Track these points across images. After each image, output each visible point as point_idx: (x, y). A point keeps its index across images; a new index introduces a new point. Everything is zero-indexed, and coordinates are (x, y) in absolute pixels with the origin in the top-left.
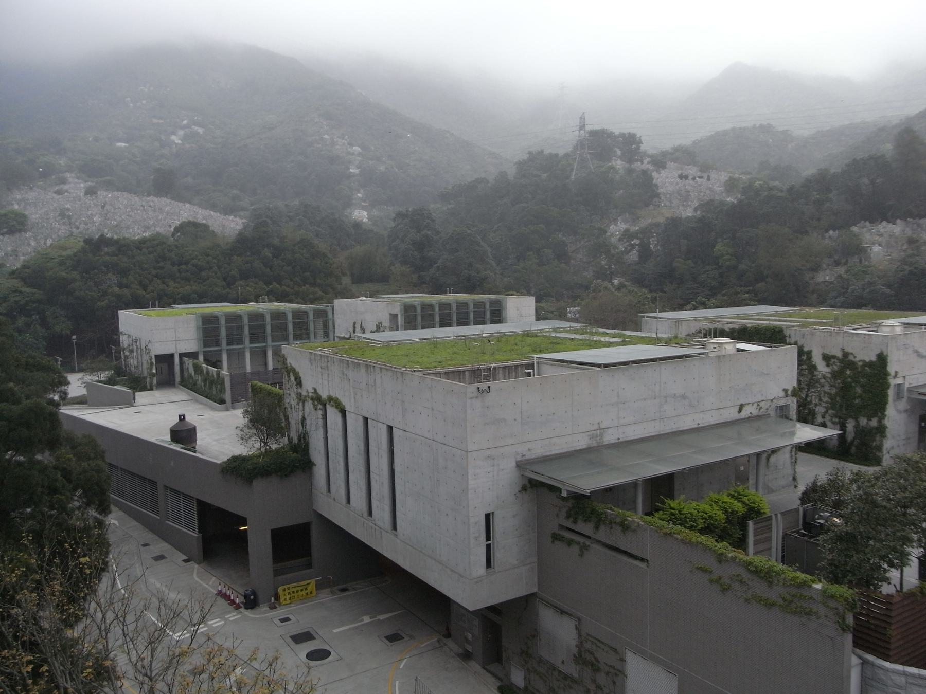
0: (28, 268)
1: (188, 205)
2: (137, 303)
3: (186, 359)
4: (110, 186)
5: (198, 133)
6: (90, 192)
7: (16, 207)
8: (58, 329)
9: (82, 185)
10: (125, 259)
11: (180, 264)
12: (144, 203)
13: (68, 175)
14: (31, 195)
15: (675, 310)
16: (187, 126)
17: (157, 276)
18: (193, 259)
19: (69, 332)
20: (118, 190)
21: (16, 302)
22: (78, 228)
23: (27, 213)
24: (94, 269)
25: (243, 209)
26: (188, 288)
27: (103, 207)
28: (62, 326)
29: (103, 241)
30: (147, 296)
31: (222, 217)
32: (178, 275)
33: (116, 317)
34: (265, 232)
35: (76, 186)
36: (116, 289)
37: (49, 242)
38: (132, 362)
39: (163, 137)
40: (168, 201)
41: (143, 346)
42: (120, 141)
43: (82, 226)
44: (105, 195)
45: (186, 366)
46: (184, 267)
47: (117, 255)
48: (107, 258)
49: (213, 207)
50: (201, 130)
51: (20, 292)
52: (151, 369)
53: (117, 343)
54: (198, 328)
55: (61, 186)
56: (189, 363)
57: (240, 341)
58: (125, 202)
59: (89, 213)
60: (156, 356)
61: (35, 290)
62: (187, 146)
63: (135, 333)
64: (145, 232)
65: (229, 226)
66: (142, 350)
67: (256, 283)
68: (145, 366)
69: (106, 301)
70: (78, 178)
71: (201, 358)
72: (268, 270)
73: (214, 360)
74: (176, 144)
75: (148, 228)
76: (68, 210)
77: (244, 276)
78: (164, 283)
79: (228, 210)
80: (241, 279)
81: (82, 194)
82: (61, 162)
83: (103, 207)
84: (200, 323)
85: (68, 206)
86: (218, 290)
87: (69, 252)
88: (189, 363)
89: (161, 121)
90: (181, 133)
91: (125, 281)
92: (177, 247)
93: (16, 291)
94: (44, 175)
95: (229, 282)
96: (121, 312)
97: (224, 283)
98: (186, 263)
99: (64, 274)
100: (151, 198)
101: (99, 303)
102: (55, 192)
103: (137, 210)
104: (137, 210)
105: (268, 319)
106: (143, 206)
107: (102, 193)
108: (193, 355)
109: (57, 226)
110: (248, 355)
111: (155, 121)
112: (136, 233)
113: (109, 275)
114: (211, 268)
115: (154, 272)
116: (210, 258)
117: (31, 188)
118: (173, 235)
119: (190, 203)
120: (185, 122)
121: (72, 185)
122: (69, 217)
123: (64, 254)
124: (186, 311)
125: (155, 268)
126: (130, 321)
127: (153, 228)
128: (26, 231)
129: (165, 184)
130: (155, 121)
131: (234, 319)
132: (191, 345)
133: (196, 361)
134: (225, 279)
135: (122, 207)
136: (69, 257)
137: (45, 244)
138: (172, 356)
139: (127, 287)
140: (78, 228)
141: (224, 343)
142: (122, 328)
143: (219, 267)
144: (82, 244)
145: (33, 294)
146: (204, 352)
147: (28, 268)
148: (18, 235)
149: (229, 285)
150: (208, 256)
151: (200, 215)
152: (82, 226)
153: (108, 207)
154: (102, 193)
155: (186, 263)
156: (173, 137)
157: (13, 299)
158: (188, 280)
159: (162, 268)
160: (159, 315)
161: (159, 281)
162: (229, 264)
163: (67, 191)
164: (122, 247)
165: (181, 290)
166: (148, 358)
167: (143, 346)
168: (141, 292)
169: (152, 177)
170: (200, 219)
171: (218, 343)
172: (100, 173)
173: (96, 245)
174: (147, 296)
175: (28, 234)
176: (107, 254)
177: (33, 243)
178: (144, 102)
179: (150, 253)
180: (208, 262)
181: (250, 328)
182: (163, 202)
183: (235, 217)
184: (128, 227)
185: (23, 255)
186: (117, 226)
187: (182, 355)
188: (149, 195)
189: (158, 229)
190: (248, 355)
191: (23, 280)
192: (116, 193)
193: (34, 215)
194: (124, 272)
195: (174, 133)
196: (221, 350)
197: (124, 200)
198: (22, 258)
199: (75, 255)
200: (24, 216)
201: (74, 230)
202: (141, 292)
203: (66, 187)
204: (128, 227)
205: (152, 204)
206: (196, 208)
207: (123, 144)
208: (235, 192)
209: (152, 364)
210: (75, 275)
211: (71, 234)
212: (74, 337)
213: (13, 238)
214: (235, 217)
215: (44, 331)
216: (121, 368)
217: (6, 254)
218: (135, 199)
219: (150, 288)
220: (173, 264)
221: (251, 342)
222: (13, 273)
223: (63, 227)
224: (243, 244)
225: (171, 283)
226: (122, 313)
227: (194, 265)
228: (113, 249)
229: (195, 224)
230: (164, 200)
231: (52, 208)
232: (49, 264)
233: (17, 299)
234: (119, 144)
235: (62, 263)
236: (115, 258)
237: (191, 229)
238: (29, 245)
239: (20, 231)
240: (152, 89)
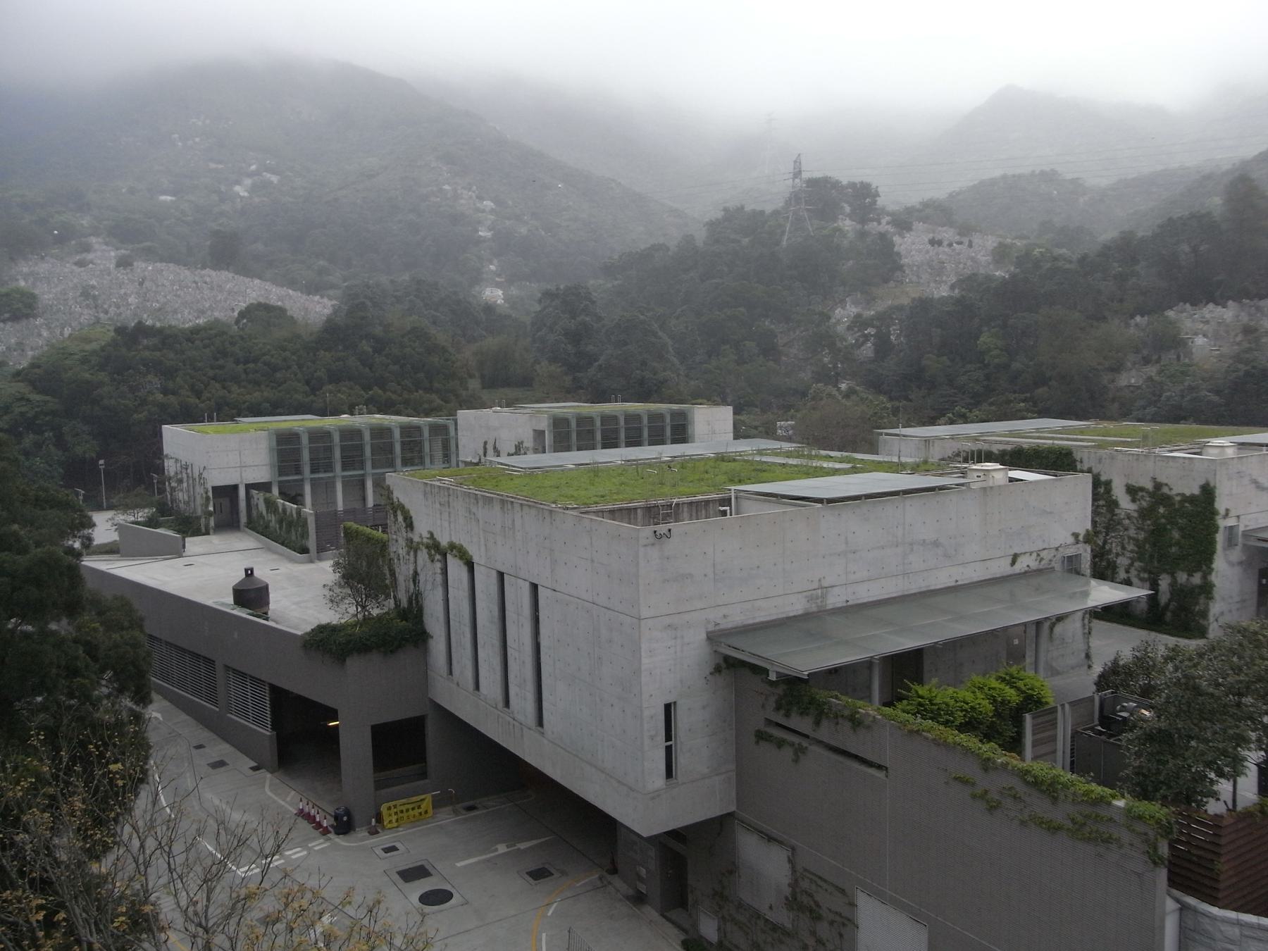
0: (39, 367)
1: (257, 281)
2: (187, 416)
3: (254, 492)
4: (150, 254)
5: (272, 183)
6: (123, 263)
7: (22, 283)
8: (79, 450)
9: (113, 254)
10: (172, 355)
11: (246, 362)
12: (197, 279)
13: (93, 240)
14: (43, 268)
15: (924, 425)
16: (257, 173)
17: (214, 378)
18: (264, 354)
19: (94, 455)
20: (161, 260)
21: (22, 414)
22: (106, 312)
23: (36, 292)
24: (129, 368)
25: (333, 286)
26: (257, 394)
27: (141, 284)
28: (85, 447)
29: (141, 330)
30: (202, 405)
31: (304, 297)
32: (243, 376)
33: (158, 435)
34: (363, 318)
35: (104, 255)
36: (159, 397)
37: (67, 332)
38: (181, 496)
39: (223, 188)
40: (231, 275)
41: (196, 475)
42: (165, 193)
43: (112, 310)
44: (143, 267)
45: (254, 501)
46: (251, 366)
47: (160, 350)
48: (147, 353)
49: (292, 283)
50: (275, 179)
51: (28, 400)
52: (207, 506)
53: (161, 470)
54: (271, 450)
55: (84, 255)
56: (259, 497)
57: (329, 467)
58: (171, 277)
59: (122, 291)
60: (213, 488)
61: (48, 398)
62: (257, 200)
63: (185, 457)
64: (198, 317)
65: (314, 309)
66: (194, 480)
67: (351, 388)
68: (199, 501)
69: (145, 413)
70: (107, 244)
71: (275, 491)
72: (367, 370)
73: (293, 493)
74: (242, 198)
75: (203, 312)
76: (93, 287)
77: (335, 378)
78: (224, 388)
79: (313, 288)
80: (330, 383)
81: (112, 266)
82: (84, 222)
83: (141, 284)
84: (274, 443)
85: (93, 282)
86: (299, 397)
87: (95, 346)
88: (259, 497)
89: (220, 166)
90: (248, 182)
91: (171, 385)
92: (242, 338)
93: (22, 399)
94: (61, 240)
95: (314, 386)
96: (165, 427)
97: (307, 388)
98: (255, 361)
99: (87, 376)
100: (207, 271)
101: (135, 416)
102: (76, 264)
103: (188, 287)
104: (188, 287)
105: (367, 437)
106: (195, 282)
107: (139, 265)
108: (264, 487)
109: (78, 309)
110: (339, 487)
111: (212, 166)
112: (186, 319)
113: (150, 377)
114: (289, 367)
115: (211, 373)
116: (288, 353)
117: (43, 258)
118: (237, 322)
119: (260, 278)
120: (253, 167)
121: (99, 253)
122: (95, 298)
123: (88, 347)
124: (255, 426)
125: (212, 368)
126: (178, 440)
127: (209, 313)
128: (35, 317)
129: (225, 252)
130: (212, 166)
131: (320, 437)
132: (261, 473)
133: (268, 495)
134: (308, 383)
135: (167, 284)
136: (94, 352)
137: (62, 334)
138: (235, 487)
139: (174, 393)
140: (106, 312)
141: (307, 470)
142: (167, 449)
143: (300, 366)
144: (113, 334)
145: (46, 402)
146: (280, 482)
147: (39, 367)
148: (24, 322)
149: (314, 391)
150: (285, 350)
151: (274, 294)
152: (112, 310)
153: (147, 284)
154: (139, 265)
155: (255, 361)
156: (237, 188)
157: (17, 410)
158: (257, 383)
159: (221, 367)
160: (218, 432)
161: (217, 385)
162: (314, 362)
163: (91, 262)
164: (167, 338)
165: (248, 397)
166: (202, 491)
167: (196, 475)
168: (193, 400)
169: (208, 243)
170: (274, 300)
171: (298, 470)
172: (137, 237)
173: (132, 335)
174: (202, 405)
175: (39, 321)
176: (147, 348)
177: (45, 334)
178: (197, 140)
179: (205, 347)
180: (285, 360)
181: (343, 449)
182: (223, 277)
183: (322, 297)
184: (175, 312)
185: (32, 349)
186: (160, 309)
187: (249, 487)
188: (204, 267)
189: (216, 314)
190: (339, 487)
191: (32, 383)
192: (158, 265)
193: (46, 295)
194: (169, 373)
195: (238, 182)
196: (302, 480)
197: (170, 273)
198: (30, 353)
199: (103, 349)
200: (33, 297)
201: (102, 315)
202: (193, 400)
203: (90, 256)
204: (175, 312)
205: (208, 279)
206: (268, 285)
207: (169, 198)
208: (321, 263)
209: (208, 498)
210: (103, 376)
211: (98, 321)
212: (101, 462)
213: (18, 326)
214: (322, 297)
215: (60, 453)
216: (165, 504)
217: (9, 348)
218: (185, 273)
219: (206, 395)
220: (237, 362)
221: (344, 469)
222: (18, 374)
223: (86, 311)
224: (333, 334)
225: (235, 388)
226: (167, 429)
227: (265, 364)
228: (155, 341)
229: (267, 308)
230: (225, 275)
231: (71, 285)
232: (67, 362)
233: (23, 409)
234: (163, 198)
235: (84, 361)
236: (158, 354)
237: (261, 313)
238: (40, 335)
239: (27, 316)
240: (208, 122)
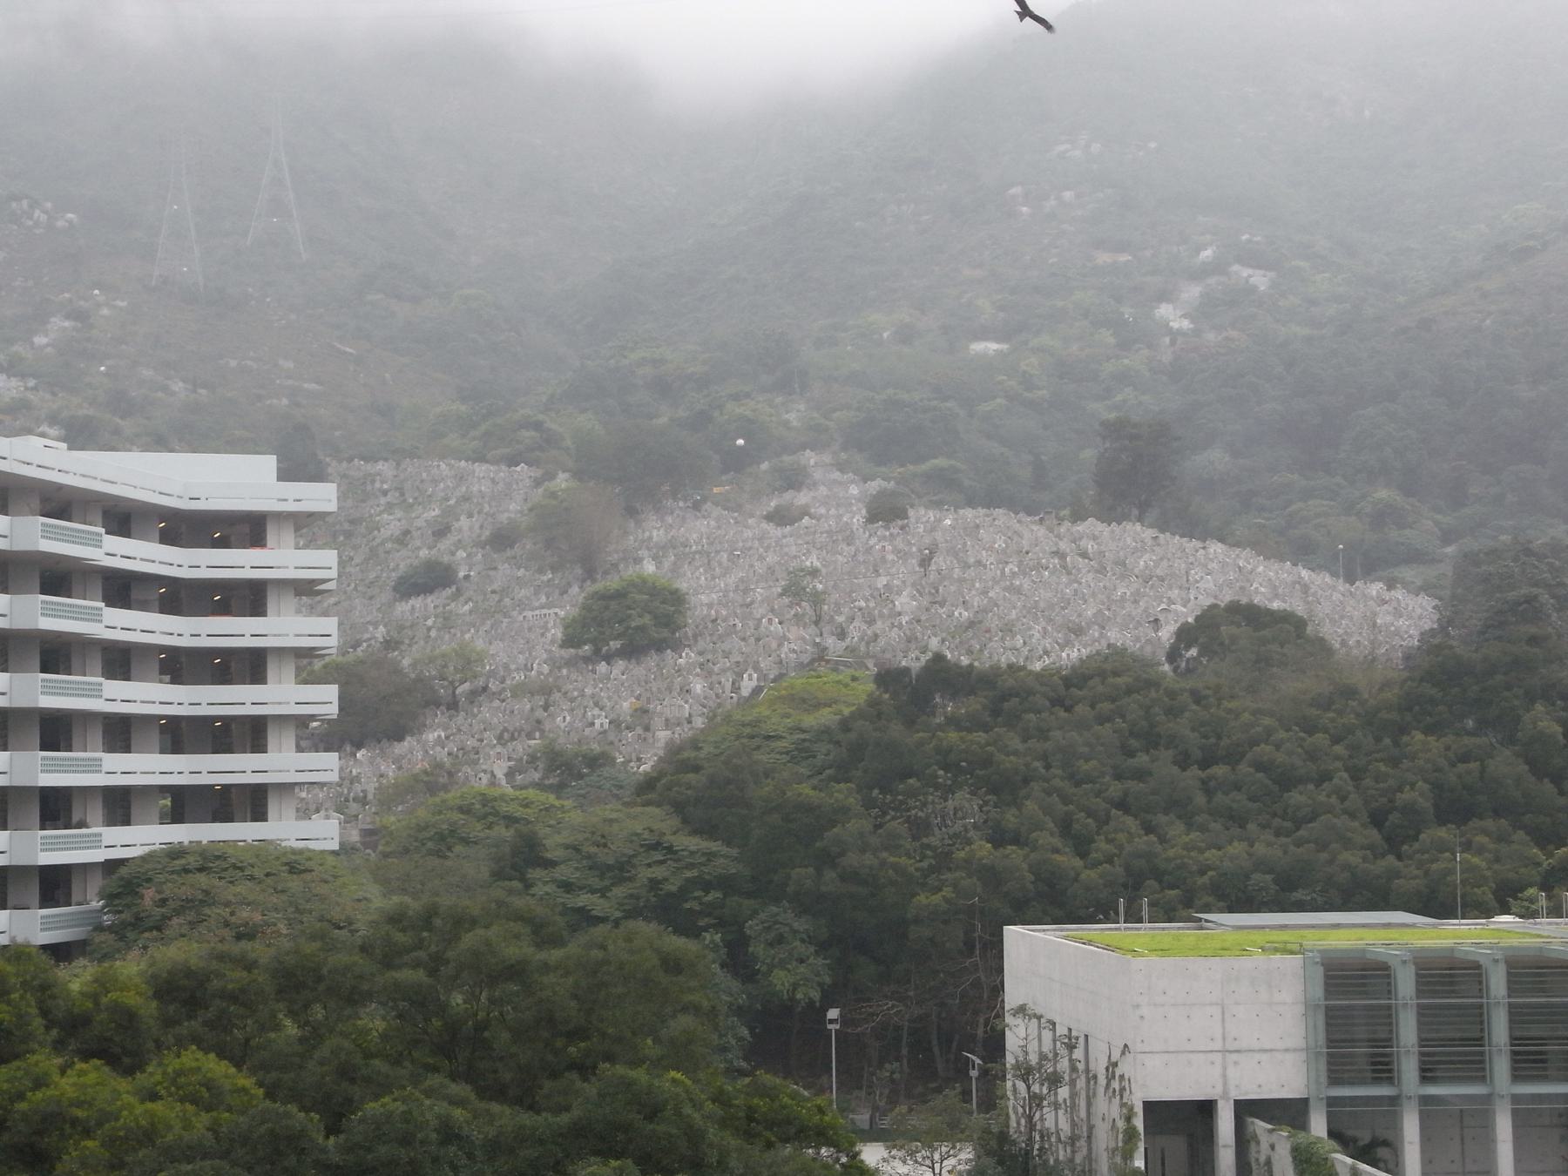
0: (697, 769)
1: (1216, 548)
2: (1059, 904)
3: (1260, 1126)
4: (947, 489)
5: (1253, 289)
6: (884, 512)
7: (649, 568)
8: (781, 980)
9: (854, 490)
10: (1015, 742)
11: (1205, 764)
12: (1063, 546)
13: (810, 458)
14: (697, 529)
15: (1222, 912)
16: (1217, 267)
17: (1123, 805)
18: (1254, 743)
19: (816, 995)
20: (971, 503)
21: (654, 884)
22: (842, 635)
23: (683, 585)
24: (906, 774)
25: (1415, 557)
26: (1237, 848)
27: (925, 562)
28: (796, 975)
29: (942, 676)
30: (1090, 875)
31: (1342, 586)
32: (1200, 799)
33: (994, 948)
34: (1533, 640)
35: (837, 495)
36: (983, 849)
37: (748, 684)
38: (1054, 1120)
39: (1127, 312)
40: (1149, 533)
41: (1099, 1067)
42: (983, 334)
43: (856, 631)
44: (931, 522)
45: (1260, 1152)
46: (1220, 770)
47: (986, 728)
48: (953, 736)
49: (1303, 552)
50: (1260, 280)
51: (670, 849)
52: (1128, 1155)
53: (995, 1046)
54: (1310, 1007)
55: (788, 495)
56: (1275, 1145)
57: (1476, 1068)
58: (1000, 543)
59: (882, 581)
60: (1149, 1106)
61: (715, 846)
62: (1211, 337)
63: (1067, 1013)
64: (1067, 644)
65: (1379, 619)
66: (1092, 1079)
67: (1501, 838)
68: (1104, 1139)
69: (947, 892)
70: (842, 467)
71: (1318, 1126)
72: (1548, 787)
73: (1365, 1137)
74: (1175, 335)
75: (1078, 631)
76: (814, 573)
77: (1455, 808)
78: (1149, 829)
79: (1361, 564)
80: (1442, 820)
81: (858, 520)
82: (792, 417)
83: (925, 562)
84: (1319, 991)
85: (813, 561)
86: (1351, 857)
87: (826, 717)
88: (1275, 1145)
89: (1124, 258)
90: (1192, 292)
91: (1011, 818)
92: (1197, 697)
93: (656, 846)
94: (736, 463)
95: (1394, 829)
96: (1011, 931)
97: (1374, 835)
98: (1233, 758)
99: (806, 790)
100: (1091, 525)
101: (922, 898)
102: (769, 518)
103: (1040, 567)
104: (1040, 567)
105: (1498, 984)
106: (1061, 555)
107: (921, 517)
108: (1287, 1113)
109: (776, 627)
110: (1504, 1127)
111: (1104, 258)
112: (1043, 648)
113: (961, 798)
114: (1324, 778)
115: (1115, 789)
116: (1320, 739)
117: (697, 506)
118: (1173, 655)
119: (1222, 540)
120: (1207, 254)
121: (823, 490)
122: (817, 599)
123: (809, 720)
124: (1258, 937)
125: (1118, 777)
126: (1050, 972)
127: (1095, 632)
128: (677, 647)
129: (1137, 476)
130: (1104, 258)
131: (1447, 977)
132: (1281, 1071)
133: (1301, 1137)
134: (1377, 820)
135: (989, 559)
136: (824, 733)
137: (736, 688)
138: (1206, 1109)
139: (1017, 840)
140: (842, 635)
141: (1409, 1068)
142: (1014, 993)
143: (1356, 775)
144: (871, 687)
145: (710, 856)
146: (1332, 1102)
147: (697, 769)
148: (652, 660)
149: (1394, 843)
150: (1311, 729)
151: (1270, 582)
152: (856, 631)
153: (940, 561)
154: (921, 517)
155: (1233, 758)
156: (1165, 311)
157: (644, 874)
158: (1237, 819)
159: (1141, 775)
160: (1163, 952)
161: (1130, 822)
162: (1394, 762)
163: (804, 512)
164: (1003, 696)
165: (1211, 855)
166: (1115, 1111)
167: (1099, 1067)
168: (1067, 860)
169: (1089, 454)
170: (1261, 595)
171: (1383, 1069)
172: (918, 451)
173: (915, 691)
174: (1090, 875)
175: (687, 657)
176: (953, 722)
177: (698, 687)
178: (1068, 195)
179: (1102, 720)
180: (1312, 756)
181: (1516, 1015)
182: (1131, 537)
183: (1391, 586)
184: (1008, 629)
185: (668, 724)
186: (971, 624)
187: (1245, 1109)
188: (1077, 517)
189: (1114, 636)
190: (1504, 1127)
191: (679, 807)
192: (969, 513)
193: (704, 593)
194: (1004, 787)
195: (1164, 296)
196: (1394, 1101)
197: (997, 530)
198: (663, 735)
199: (845, 725)
200: (677, 599)
201: (830, 641)
202: (1067, 860)
203: (802, 498)
204: (1008, 629)
205: (1091, 547)
206: (1245, 558)
207: (993, 346)
208: (1383, 494)
209: (1131, 1134)
210: (843, 794)
211: (821, 655)
212: (833, 1013)
213: (639, 671)
214: (1391, 586)
215: (735, 985)
216: (1003, 1137)
217: (615, 723)
218: (1032, 532)
219: (1101, 846)
220: (1183, 762)
221: (1517, 1077)
222: (648, 785)
223: (794, 632)
224: (1442, 686)
225: (1176, 830)
226: (1011, 931)
227: (1260, 766)
228: (974, 704)
229: (1248, 615)
230: (1134, 533)
231: (760, 568)
232: (757, 756)
233: (658, 872)
234: (978, 347)
235: (801, 752)
236: (980, 737)
237: (1228, 630)
238: (686, 691)
239: (660, 646)
240: (1096, 148)
